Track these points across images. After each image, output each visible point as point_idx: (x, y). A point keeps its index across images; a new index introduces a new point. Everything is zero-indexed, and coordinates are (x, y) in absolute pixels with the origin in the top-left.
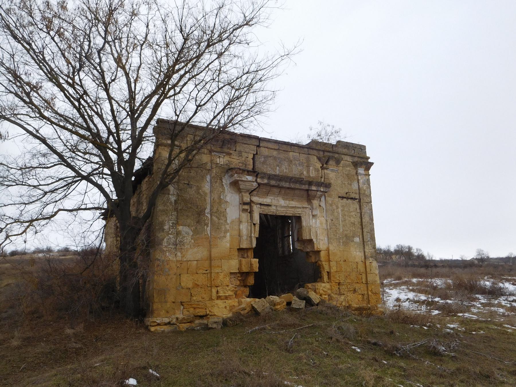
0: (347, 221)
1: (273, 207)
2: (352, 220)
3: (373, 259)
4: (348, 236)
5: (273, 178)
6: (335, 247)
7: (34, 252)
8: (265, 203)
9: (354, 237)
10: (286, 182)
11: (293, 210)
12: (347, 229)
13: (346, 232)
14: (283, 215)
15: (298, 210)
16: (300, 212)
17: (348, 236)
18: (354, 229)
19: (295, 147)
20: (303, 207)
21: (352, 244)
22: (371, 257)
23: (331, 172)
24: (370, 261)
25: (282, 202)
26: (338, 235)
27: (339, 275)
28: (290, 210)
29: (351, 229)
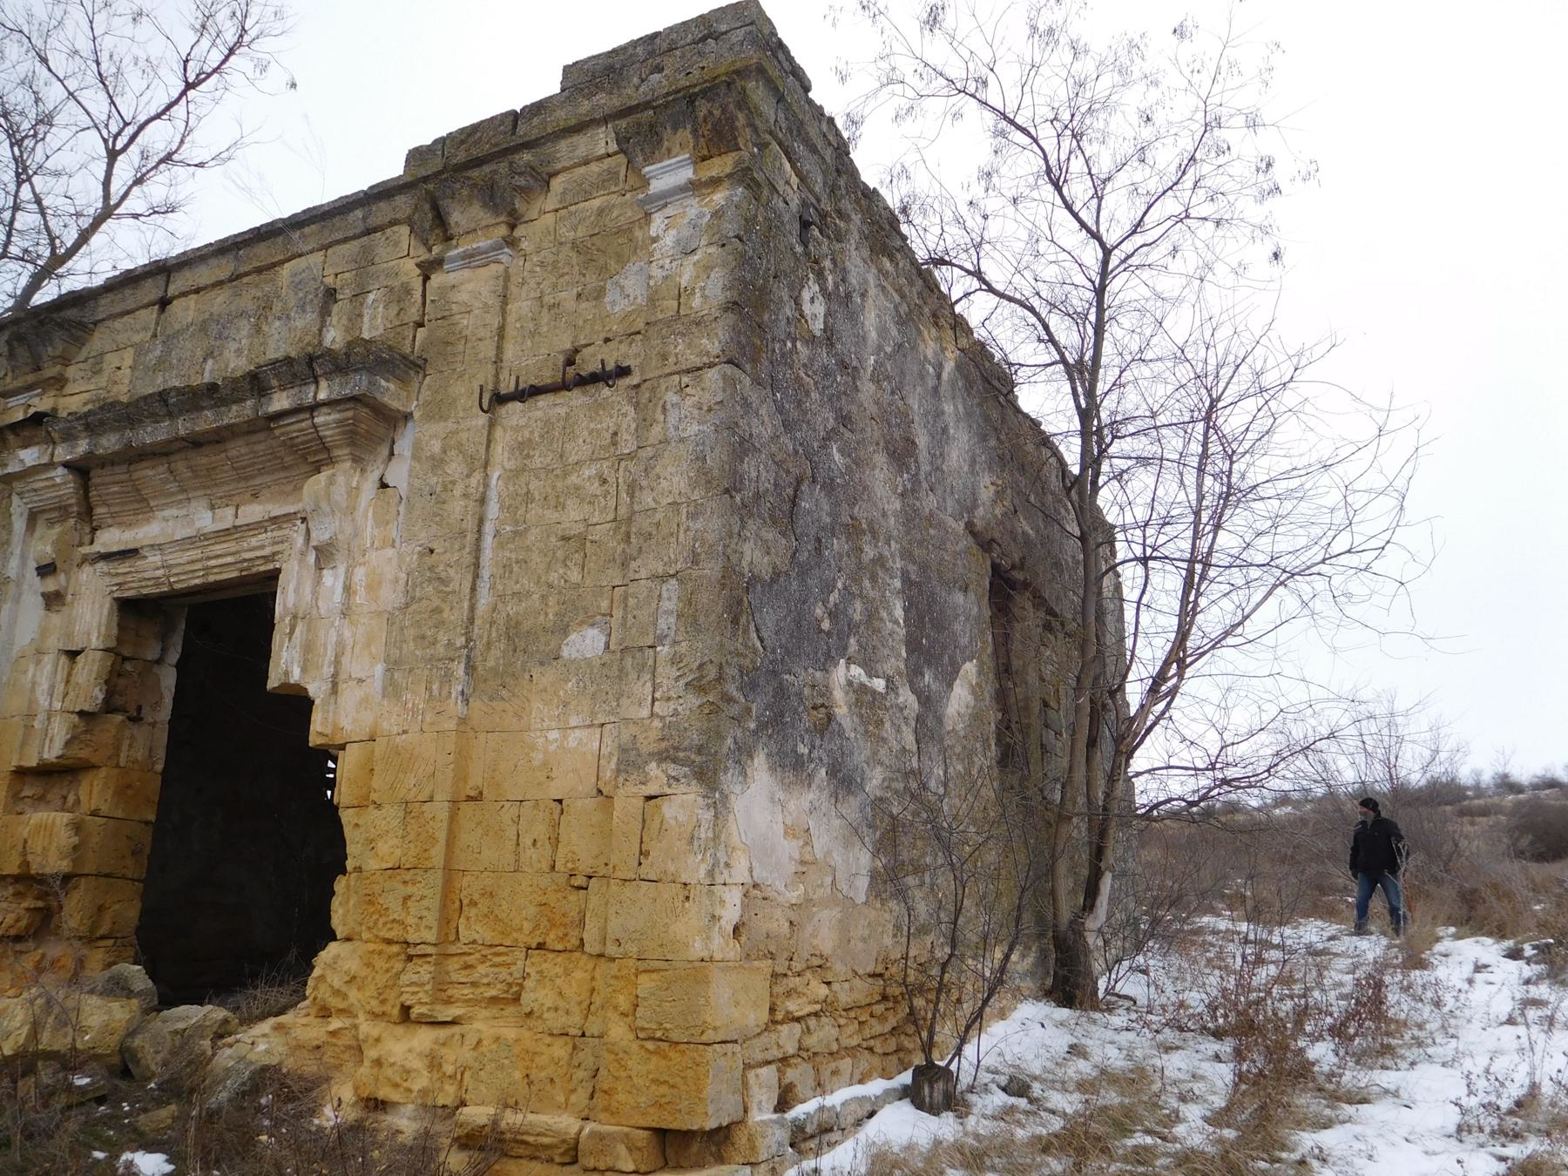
0: (533, 535)
1: (151, 559)
2: (572, 516)
3: (673, 769)
4: (526, 626)
5: (102, 423)
6: (414, 711)
7: (1536, 787)
8: (115, 549)
9: (565, 631)
10: (156, 418)
11: (231, 546)
12: (527, 583)
13: (512, 608)
14: (197, 581)
15: (254, 542)
16: (267, 552)
17: (526, 626)
18: (575, 576)
19: (307, 230)
20: (274, 520)
21: (545, 677)
22: (663, 757)
23: (466, 273)
24: (652, 789)
25: (204, 519)
26: (443, 638)
27: (410, 889)
28: (218, 549)
29: (553, 577)
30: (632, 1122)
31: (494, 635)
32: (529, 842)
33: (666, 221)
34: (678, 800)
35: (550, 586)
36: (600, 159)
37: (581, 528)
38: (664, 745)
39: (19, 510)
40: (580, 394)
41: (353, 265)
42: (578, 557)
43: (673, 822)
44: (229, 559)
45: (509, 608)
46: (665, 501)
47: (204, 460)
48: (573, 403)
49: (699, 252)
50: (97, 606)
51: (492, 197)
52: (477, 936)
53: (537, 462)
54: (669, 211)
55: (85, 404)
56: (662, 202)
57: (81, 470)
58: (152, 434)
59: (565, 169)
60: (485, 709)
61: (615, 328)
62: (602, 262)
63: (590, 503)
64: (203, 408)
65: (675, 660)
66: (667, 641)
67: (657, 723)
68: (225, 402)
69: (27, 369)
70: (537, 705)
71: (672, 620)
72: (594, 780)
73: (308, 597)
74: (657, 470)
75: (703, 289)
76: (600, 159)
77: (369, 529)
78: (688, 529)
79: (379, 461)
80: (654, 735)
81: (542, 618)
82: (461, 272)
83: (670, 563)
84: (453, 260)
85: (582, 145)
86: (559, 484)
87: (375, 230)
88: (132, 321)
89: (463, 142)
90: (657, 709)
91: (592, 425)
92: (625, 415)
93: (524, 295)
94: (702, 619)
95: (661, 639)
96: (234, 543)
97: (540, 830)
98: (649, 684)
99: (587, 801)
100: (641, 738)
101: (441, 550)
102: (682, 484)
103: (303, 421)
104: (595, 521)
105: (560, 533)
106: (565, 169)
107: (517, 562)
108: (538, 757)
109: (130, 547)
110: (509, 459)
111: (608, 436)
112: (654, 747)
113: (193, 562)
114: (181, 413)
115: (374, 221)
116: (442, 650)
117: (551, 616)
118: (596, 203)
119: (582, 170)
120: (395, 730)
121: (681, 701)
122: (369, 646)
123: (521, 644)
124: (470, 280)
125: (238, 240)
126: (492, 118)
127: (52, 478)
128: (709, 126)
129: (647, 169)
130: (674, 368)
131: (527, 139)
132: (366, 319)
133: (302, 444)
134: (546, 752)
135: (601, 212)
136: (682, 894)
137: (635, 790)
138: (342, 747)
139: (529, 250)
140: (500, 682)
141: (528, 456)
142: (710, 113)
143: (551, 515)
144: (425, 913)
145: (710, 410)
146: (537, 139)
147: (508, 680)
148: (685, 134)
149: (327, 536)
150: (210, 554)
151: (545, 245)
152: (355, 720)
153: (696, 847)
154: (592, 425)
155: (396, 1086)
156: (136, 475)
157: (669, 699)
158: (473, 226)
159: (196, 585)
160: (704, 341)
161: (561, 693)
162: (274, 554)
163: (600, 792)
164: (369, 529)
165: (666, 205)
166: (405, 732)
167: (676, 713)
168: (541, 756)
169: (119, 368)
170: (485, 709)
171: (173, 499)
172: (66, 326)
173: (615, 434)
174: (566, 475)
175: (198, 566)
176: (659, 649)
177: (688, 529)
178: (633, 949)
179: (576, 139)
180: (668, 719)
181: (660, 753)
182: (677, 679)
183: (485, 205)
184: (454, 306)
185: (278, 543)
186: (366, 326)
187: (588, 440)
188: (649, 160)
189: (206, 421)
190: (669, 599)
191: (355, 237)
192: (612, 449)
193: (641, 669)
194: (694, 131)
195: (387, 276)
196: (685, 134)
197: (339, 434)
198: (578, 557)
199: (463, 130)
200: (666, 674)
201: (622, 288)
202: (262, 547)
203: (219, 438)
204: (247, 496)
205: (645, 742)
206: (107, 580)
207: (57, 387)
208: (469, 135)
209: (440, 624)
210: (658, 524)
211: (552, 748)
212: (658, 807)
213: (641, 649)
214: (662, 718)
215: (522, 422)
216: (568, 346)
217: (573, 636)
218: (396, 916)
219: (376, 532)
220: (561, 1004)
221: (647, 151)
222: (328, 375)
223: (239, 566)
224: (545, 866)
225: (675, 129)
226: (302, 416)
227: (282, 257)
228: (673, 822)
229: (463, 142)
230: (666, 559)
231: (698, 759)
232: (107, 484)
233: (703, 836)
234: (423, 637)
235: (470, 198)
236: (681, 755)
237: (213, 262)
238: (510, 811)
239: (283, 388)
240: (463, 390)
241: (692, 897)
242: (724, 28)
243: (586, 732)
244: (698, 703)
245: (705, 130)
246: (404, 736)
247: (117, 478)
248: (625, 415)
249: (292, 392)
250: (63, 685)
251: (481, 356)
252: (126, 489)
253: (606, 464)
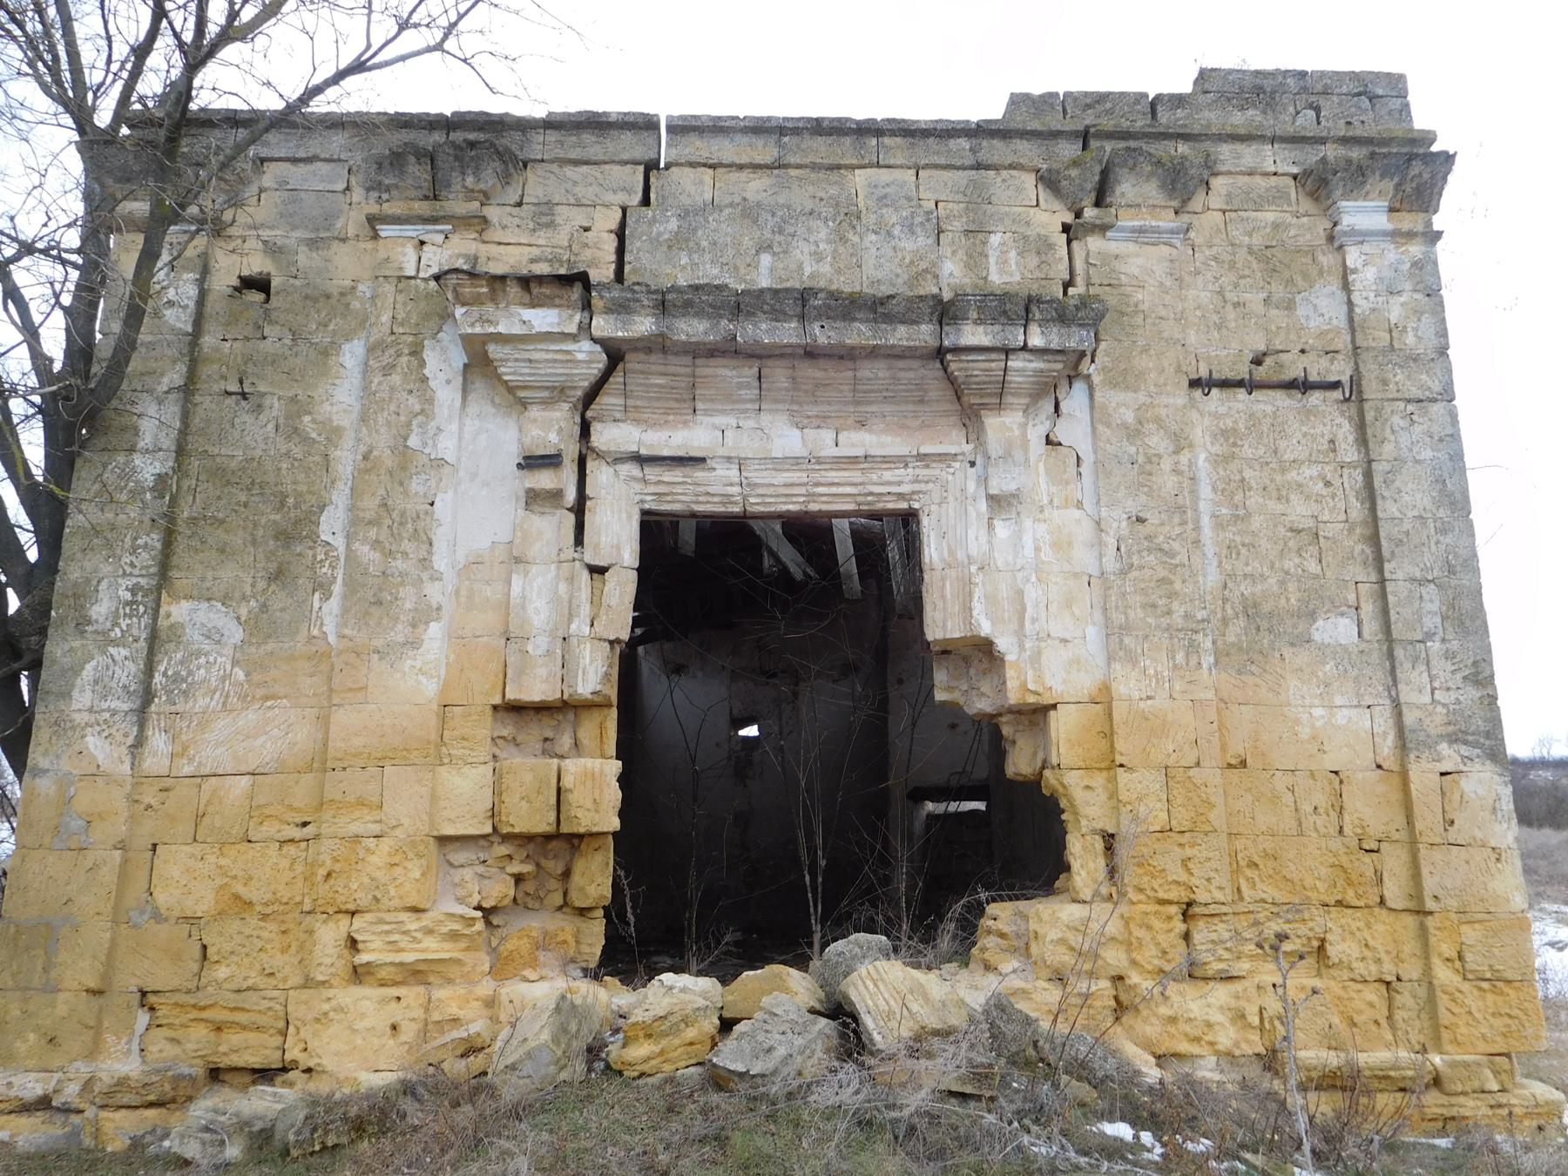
0: (1256, 522)
1: (719, 472)
2: (1299, 511)
3: (1465, 750)
9: (1312, 616)
10: (777, 315)
11: (856, 476)
13: (1246, 588)
14: (792, 507)
15: (887, 476)
16: (905, 489)
17: (1266, 608)
18: (1313, 567)
22: (1453, 739)
23: (1132, 247)
25: (787, 439)
28: (833, 476)
30: (1480, 1050)
31: (1230, 611)
32: (1309, 809)
33: (1364, 257)
34: (1475, 776)
35: (1287, 573)
36: (1266, 174)
37: (1310, 523)
38: (1451, 728)
39: (442, 376)
40: (1284, 396)
41: (960, 197)
42: (1313, 550)
43: (1473, 796)
44: (849, 490)
45: (1242, 588)
46: (1410, 514)
47: (819, 374)
48: (1279, 403)
49: (1405, 295)
50: (624, 516)
51: (1173, 182)
52: (1264, 896)
53: (1247, 451)
54: (1366, 248)
55: (532, 261)
56: (1361, 239)
57: (615, 354)
58: (762, 331)
59: (1229, 173)
60: (1233, 681)
61: (1311, 341)
62: (1287, 274)
63: (1316, 501)
64: (854, 319)
65: (1449, 656)
66: (1437, 638)
67: (1439, 709)
68: (890, 319)
69: (413, 193)
70: (1293, 683)
71: (1438, 620)
72: (1371, 755)
73: (986, 547)
74: (1397, 483)
75: (1416, 330)
76: (1266, 174)
77: (1043, 486)
78: (1437, 542)
79: (1043, 416)
80: (1439, 719)
81: (1283, 601)
82: (1125, 244)
83: (1425, 569)
84: (1122, 230)
85: (1248, 155)
86: (1278, 478)
87: (988, 168)
88: (598, 175)
89: (1089, 106)
90: (1438, 695)
91: (1304, 429)
92: (1339, 426)
93: (856, 239)
94: (1468, 623)
95: (1430, 636)
96: (858, 474)
97: (1321, 798)
98: (1425, 675)
99: (1369, 773)
100: (1427, 721)
101: (1156, 522)
102: (1425, 500)
103: (993, 361)
104: (1325, 519)
105: (1289, 526)
106: (1229, 173)
107: (1243, 545)
108: (1305, 733)
109: (693, 454)
110: (1212, 443)
111: (1325, 441)
112: (1440, 730)
113: (792, 485)
114: (818, 317)
115: (983, 156)
116: (1180, 621)
117: (1293, 601)
118: (1270, 216)
119: (1246, 178)
120: (1136, 695)
121: (1461, 692)
122: (1069, 606)
123: (1264, 624)
124: (1138, 256)
125: (789, 125)
126: (1122, 94)
127: (568, 352)
128: (1414, 185)
129: (1344, 203)
130: (1395, 395)
131: (1188, 131)
132: (992, 260)
133: (978, 383)
134: (1313, 726)
135: (1276, 226)
136: (1494, 856)
137: (1430, 766)
138: (1054, 707)
139: (1199, 241)
140: (1246, 657)
141: (1235, 444)
142: (1420, 175)
143: (1275, 506)
144: (1212, 874)
145: (1441, 440)
146: (1200, 135)
147: (1256, 657)
148: (1389, 185)
149: (1012, 487)
150: (823, 480)
151: (1217, 241)
152: (1064, 681)
153: (1499, 816)
154: (1304, 429)
155: (1197, 1040)
156: (699, 371)
157: (1448, 689)
158: (1140, 200)
159: (788, 511)
160: (1424, 377)
161: (1320, 674)
162: (913, 493)
163: (1379, 767)
164: (1043, 486)
165: (1362, 243)
166: (1149, 698)
167: (1458, 702)
168: (1308, 730)
169: (587, 229)
170: (1233, 681)
171: (737, 406)
172: (506, 158)
173: (1332, 441)
174: (1283, 471)
175: (802, 490)
176: (1429, 644)
177: (1437, 542)
178: (1453, 903)
179: (1239, 147)
180: (1451, 707)
181: (1449, 735)
182: (1453, 672)
183: (1162, 186)
184: (1123, 277)
185: (920, 482)
186: (993, 268)
187: (1303, 442)
188: (1347, 195)
189: (859, 334)
190: (1431, 601)
191: (963, 168)
192: (1331, 455)
193: (1415, 660)
194: (1398, 187)
195: (1014, 221)
196: (1389, 185)
197: (1034, 383)
198: (1313, 550)
199: (1086, 94)
200: (1442, 668)
201: (1315, 306)
202: (899, 483)
203: (846, 355)
204: (850, 421)
205: (1432, 725)
206: (638, 487)
207: (479, 228)
208: (1098, 102)
209: (1172, 595)
210: (1407, 533)
211: (1319, 724)
212: (1457, 783)
213: (1411, 643)
214: (1444, 705)
215: (1222, 410)
216: (1262, 348)
217: (1320, 623)
218: (1175, 877)
219: (1054, 489)
220: (1367, 953)
221: (1348, 188)
222: (1043, 323)
223: (860, 499)
224: (1333, 830)
225: (1383, 176)
226: (994, 356)
227: (854, 161)
228: (1473, 796)
229: (1089, 106)
230: (1422, 565)
231: (1488, 743)
232: (641, 374)
233: (1504, 808)
234: (1154, 606)
235: (1151, 174)
236: (1470, 738)
237: (744, 140)
238: (1281, 782)
239: (979, 322)
240: (1151, 365)
241: (1503, 858)
242: (1380, 92)
243: (1354, 712)
244: (1479, 695)
245: (1408, 188)
246: (1149, 702)
247: (672, 369)
248: (1339, 426)
249: (997, 328)
250: (588, 605)
251: (1165, 335)
252: (677, 384)
253: (1327, 468)
